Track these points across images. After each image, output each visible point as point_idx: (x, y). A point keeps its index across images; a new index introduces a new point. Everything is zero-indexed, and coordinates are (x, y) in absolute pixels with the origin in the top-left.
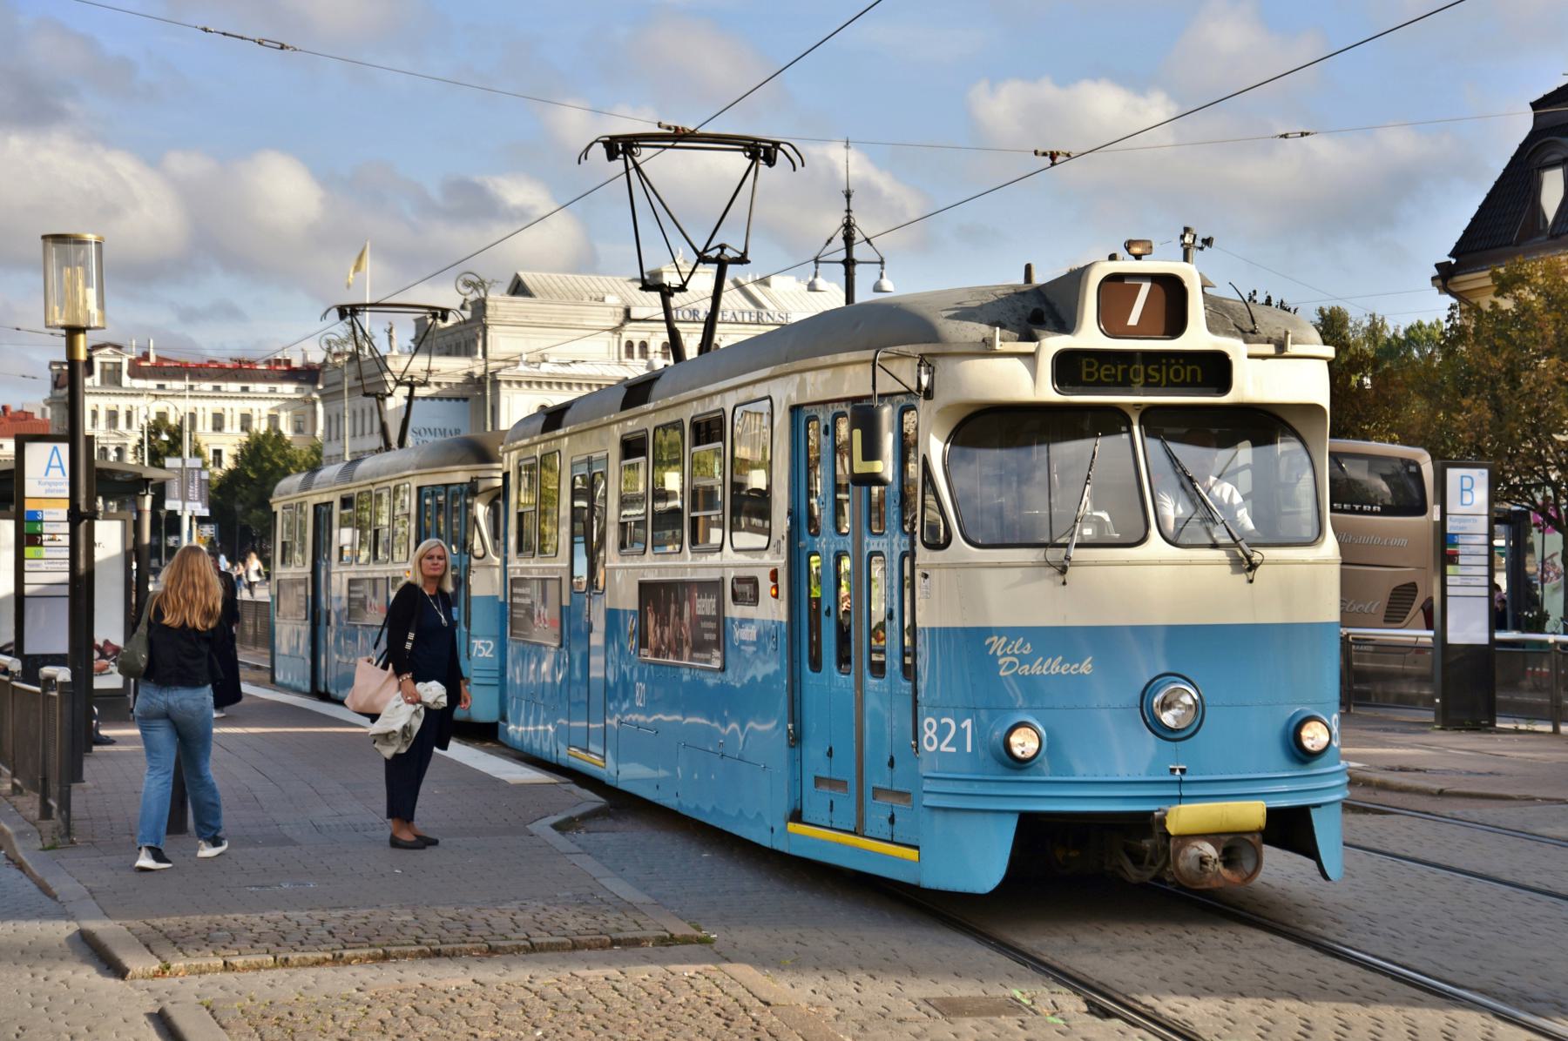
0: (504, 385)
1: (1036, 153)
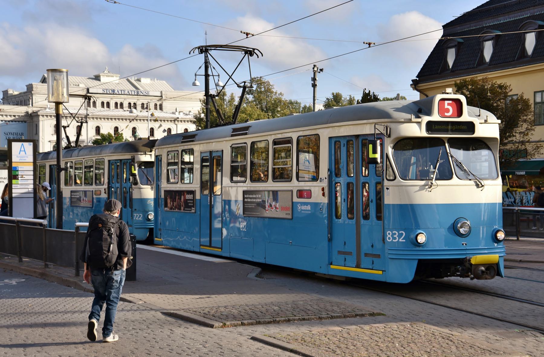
0: (41, 117)
1: (241, 32)
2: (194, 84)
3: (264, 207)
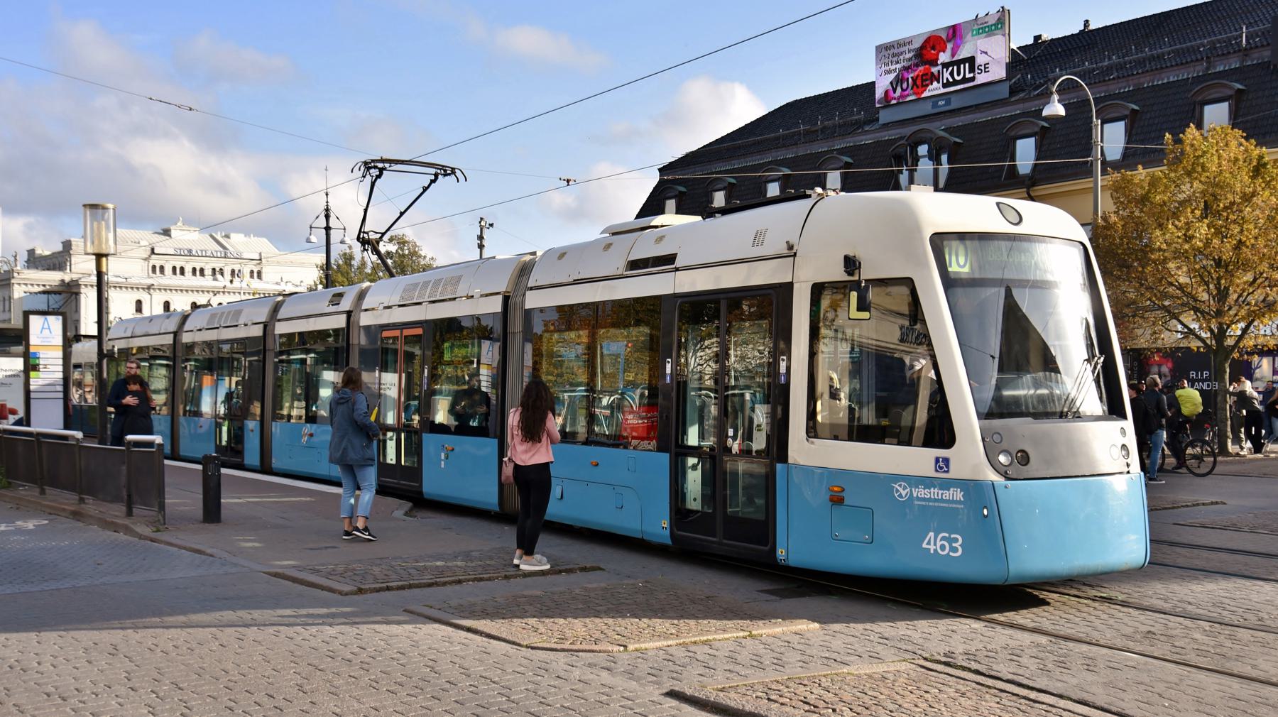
2: (308, 241)
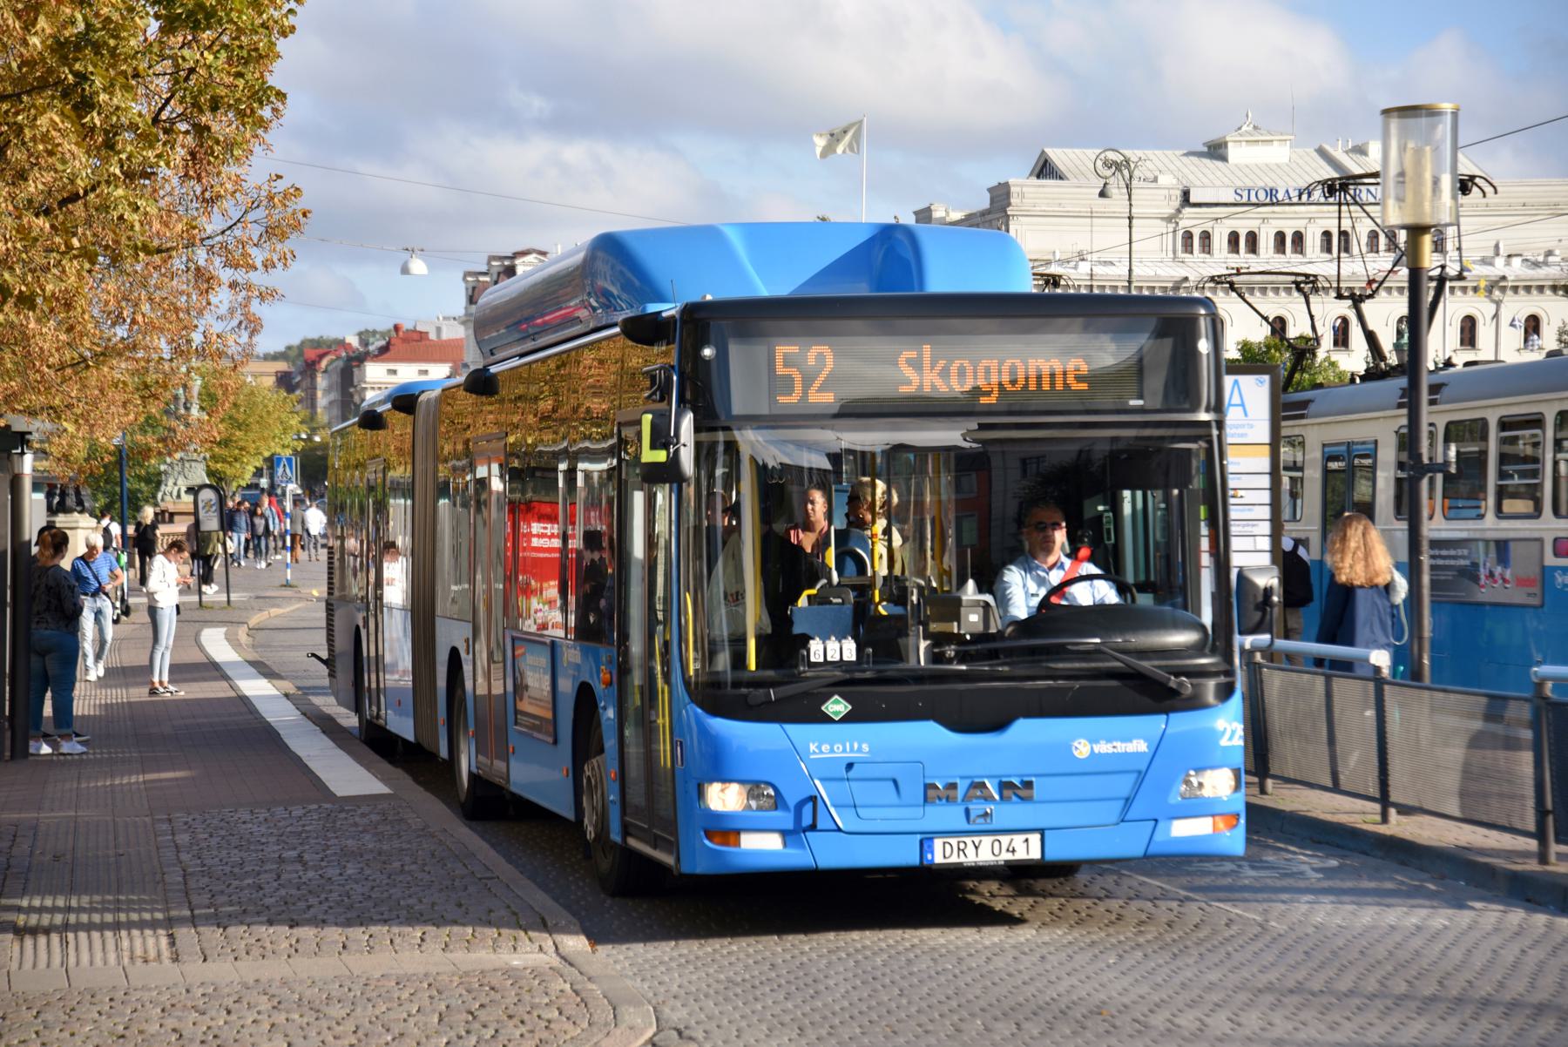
3: (1476, 579)
